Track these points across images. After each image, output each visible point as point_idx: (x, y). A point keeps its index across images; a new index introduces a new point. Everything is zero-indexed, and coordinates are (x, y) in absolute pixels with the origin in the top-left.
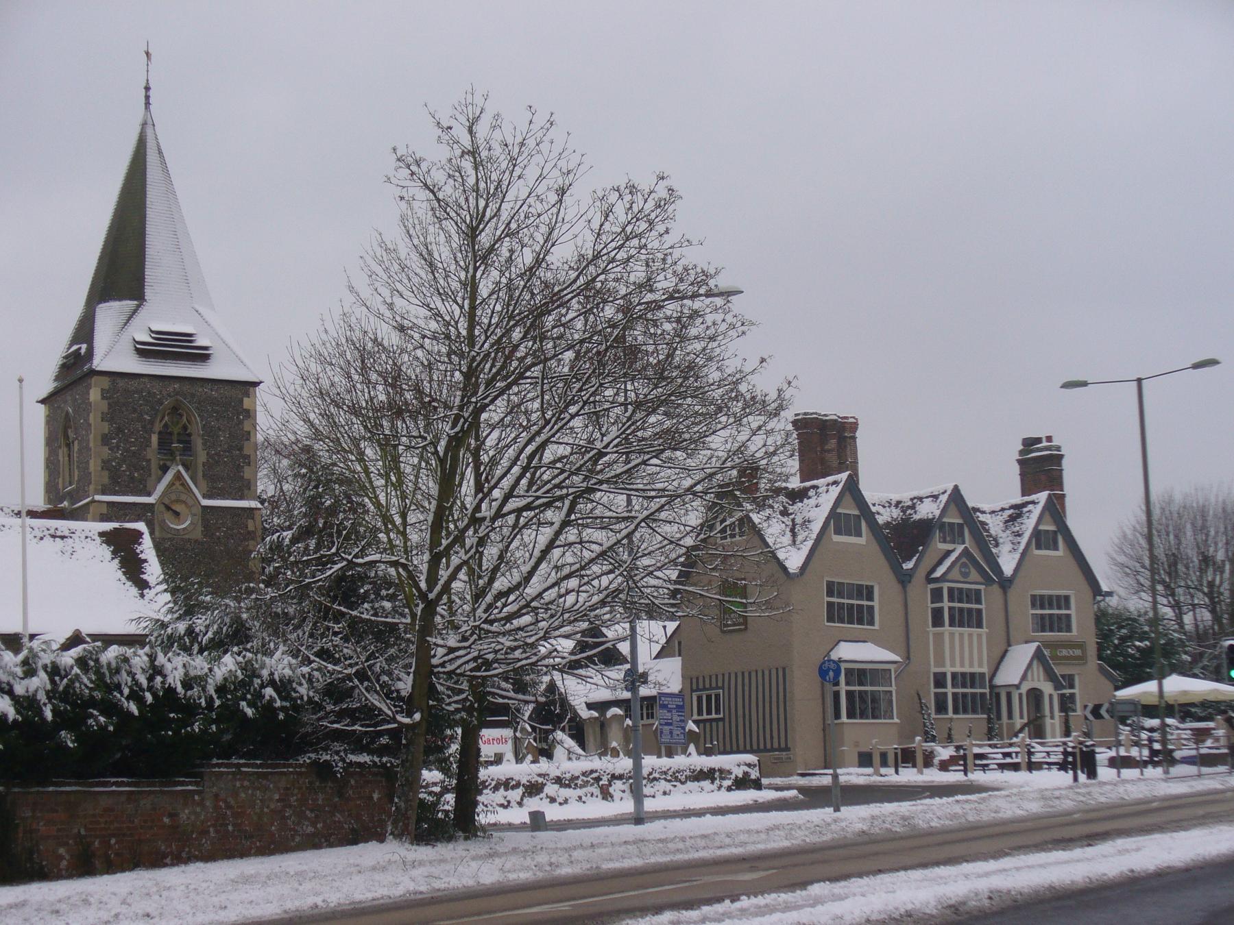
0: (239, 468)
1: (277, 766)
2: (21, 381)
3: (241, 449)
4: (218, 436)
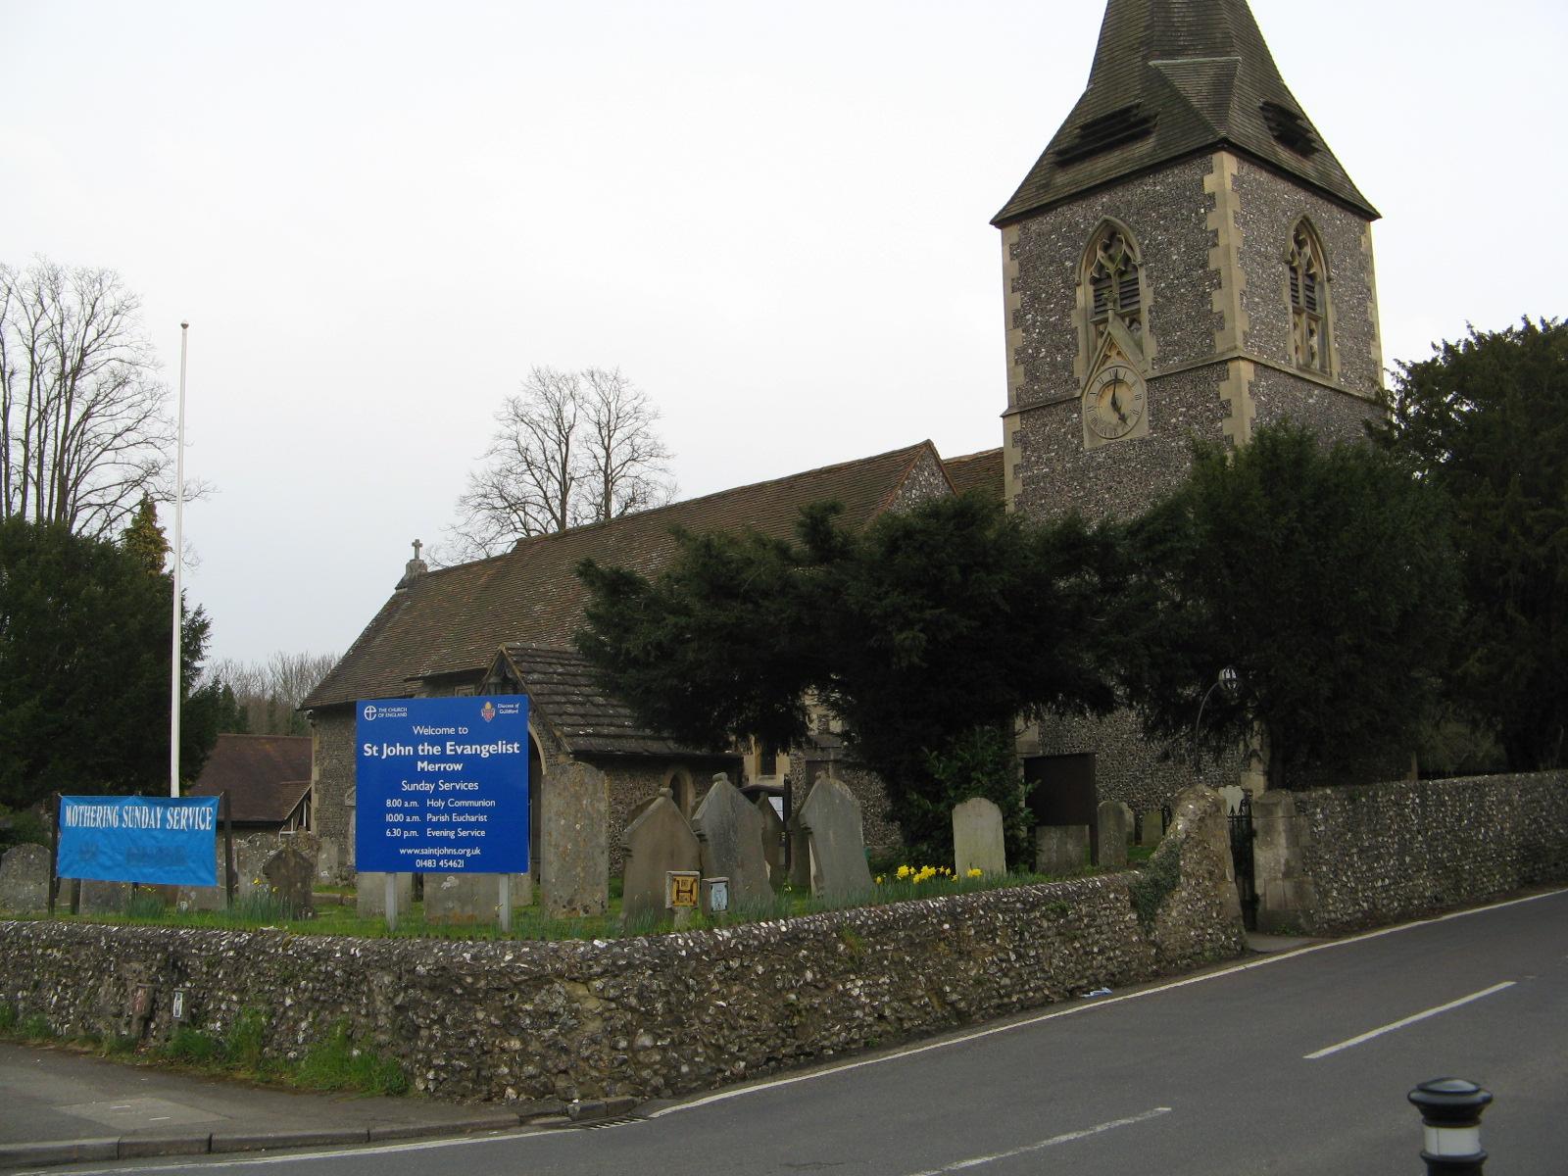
0: (1204, 298)
2: (185, 326)
3: (1204, 265)
4: (1168, 256)
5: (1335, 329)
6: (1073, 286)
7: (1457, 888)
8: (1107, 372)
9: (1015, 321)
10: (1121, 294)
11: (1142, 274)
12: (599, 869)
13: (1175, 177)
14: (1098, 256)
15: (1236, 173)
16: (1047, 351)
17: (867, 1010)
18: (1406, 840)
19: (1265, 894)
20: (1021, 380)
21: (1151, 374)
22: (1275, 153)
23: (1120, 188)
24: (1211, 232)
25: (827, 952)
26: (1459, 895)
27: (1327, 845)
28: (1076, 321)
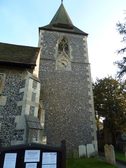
1: (34, 156)
3: (83, 49)
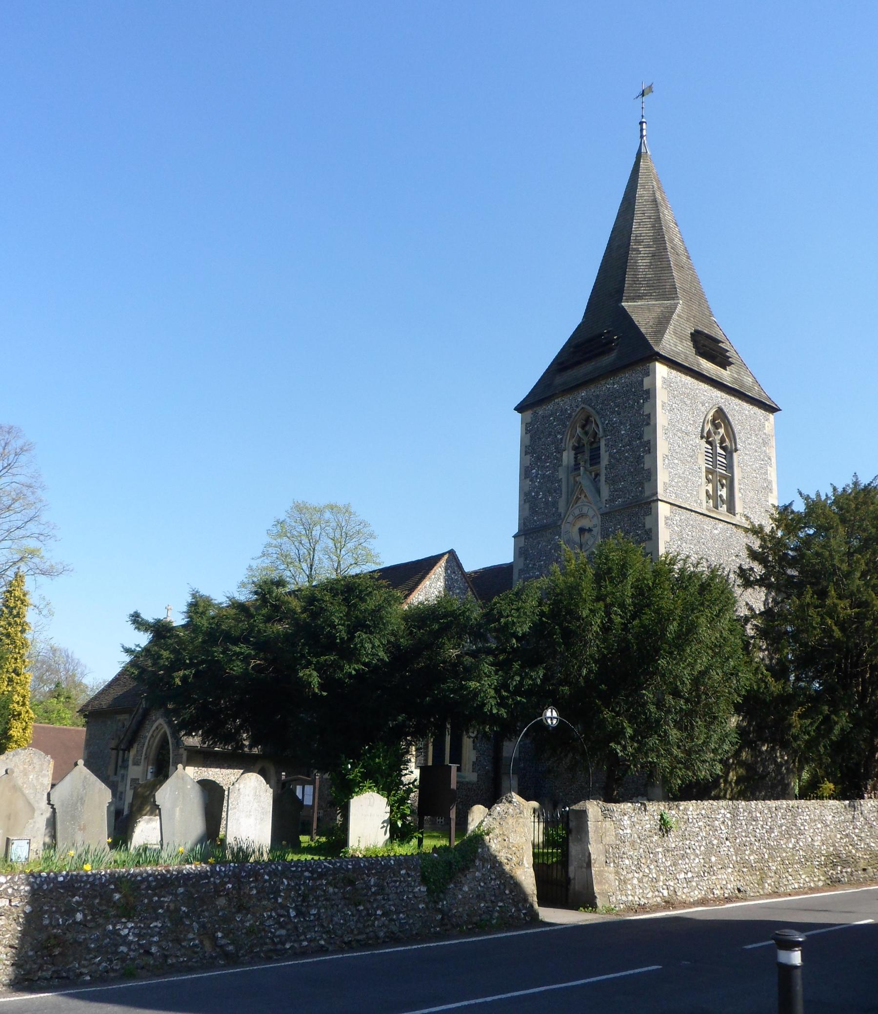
3: (640, 438)
5: (740, 484)
6: (560, 451)
7: (762, 881)
8: (578, 509)
9: (525, 474)
10: (591, 456)
11: (603, 443)
12: (37, 825)
13: (626, 378)
14: (578, 431)
15: (666, 376)
16: (543, 494)
17: (132, 947)
18: (713, 845)
19: (574, 879)
20: (527, 513)
21: (604, 510)
22: (699, 365)
23: (592, 386)
24: (646, 415)
25: (101, 899)
26: (763, 889)
27: (633, 844)
28: (562, 474)
